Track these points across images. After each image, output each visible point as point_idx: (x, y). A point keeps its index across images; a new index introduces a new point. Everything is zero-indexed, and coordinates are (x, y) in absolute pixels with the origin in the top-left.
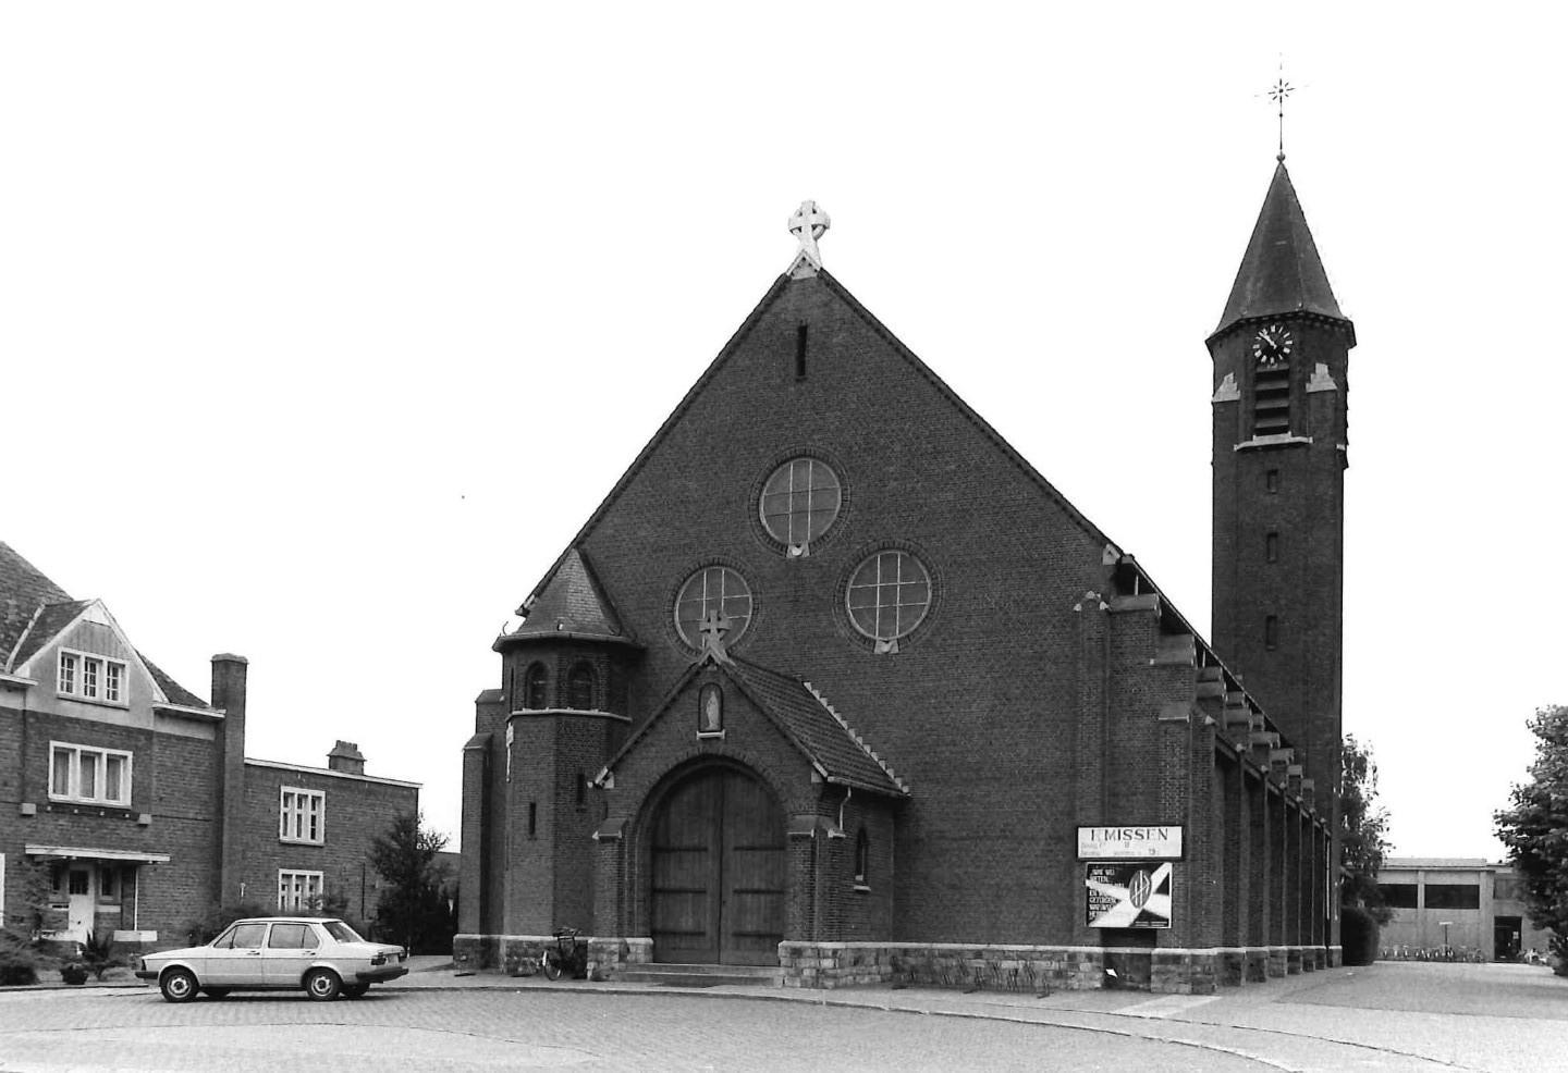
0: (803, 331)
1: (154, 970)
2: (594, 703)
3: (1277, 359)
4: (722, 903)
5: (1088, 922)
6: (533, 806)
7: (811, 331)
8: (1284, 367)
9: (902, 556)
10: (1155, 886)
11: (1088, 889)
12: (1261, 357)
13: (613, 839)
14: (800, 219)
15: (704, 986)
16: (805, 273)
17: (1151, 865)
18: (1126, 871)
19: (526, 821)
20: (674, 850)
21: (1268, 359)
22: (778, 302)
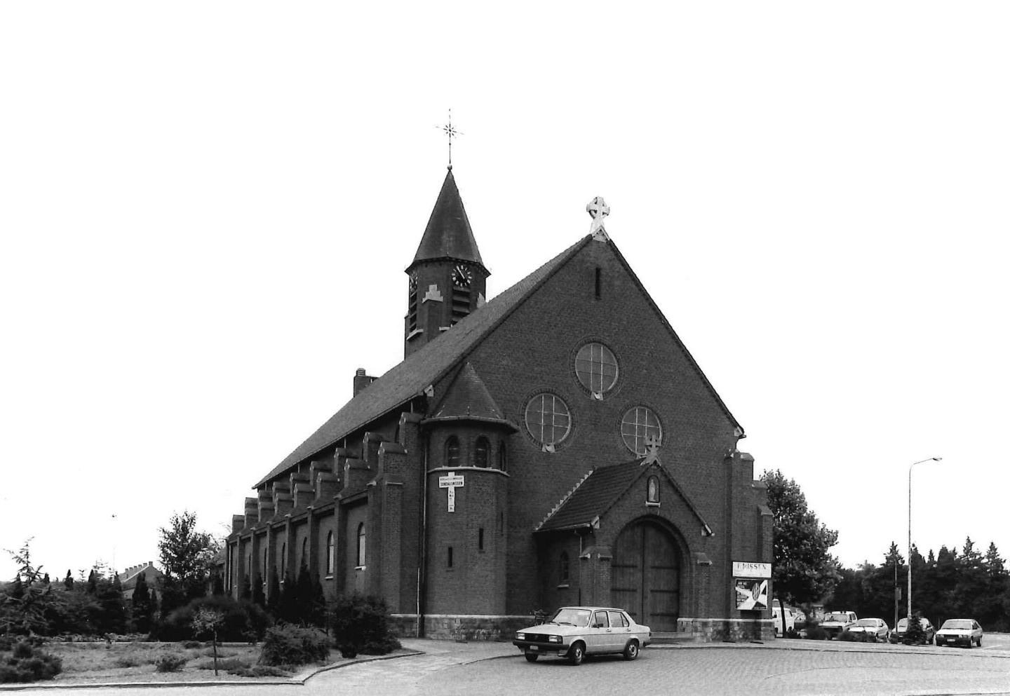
0: (598, 270)
1: (567, 643)
2: (488, 463)
3: (464, 285)
4: (644, 597)
5: (737, 607)
6: (481, 531)
7: (603, 272)
8: (467, 290)
9: (545, 396)
10: (762, 590)
11: (737, 592)
12: (456, 281)
13: (608, 559)
14: (596, 205)
15: (666, 643)
16: (600, 238)
17: (760, 581)
18: (751, 583)
19: (477, 540)
20: (619, 566)
21: (459, 284)
22: (585, 248)
